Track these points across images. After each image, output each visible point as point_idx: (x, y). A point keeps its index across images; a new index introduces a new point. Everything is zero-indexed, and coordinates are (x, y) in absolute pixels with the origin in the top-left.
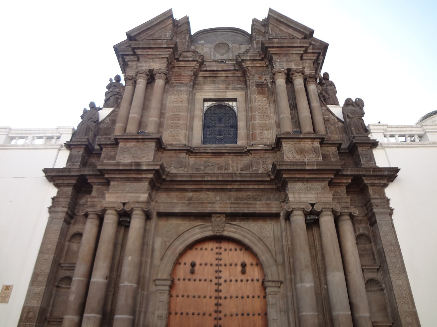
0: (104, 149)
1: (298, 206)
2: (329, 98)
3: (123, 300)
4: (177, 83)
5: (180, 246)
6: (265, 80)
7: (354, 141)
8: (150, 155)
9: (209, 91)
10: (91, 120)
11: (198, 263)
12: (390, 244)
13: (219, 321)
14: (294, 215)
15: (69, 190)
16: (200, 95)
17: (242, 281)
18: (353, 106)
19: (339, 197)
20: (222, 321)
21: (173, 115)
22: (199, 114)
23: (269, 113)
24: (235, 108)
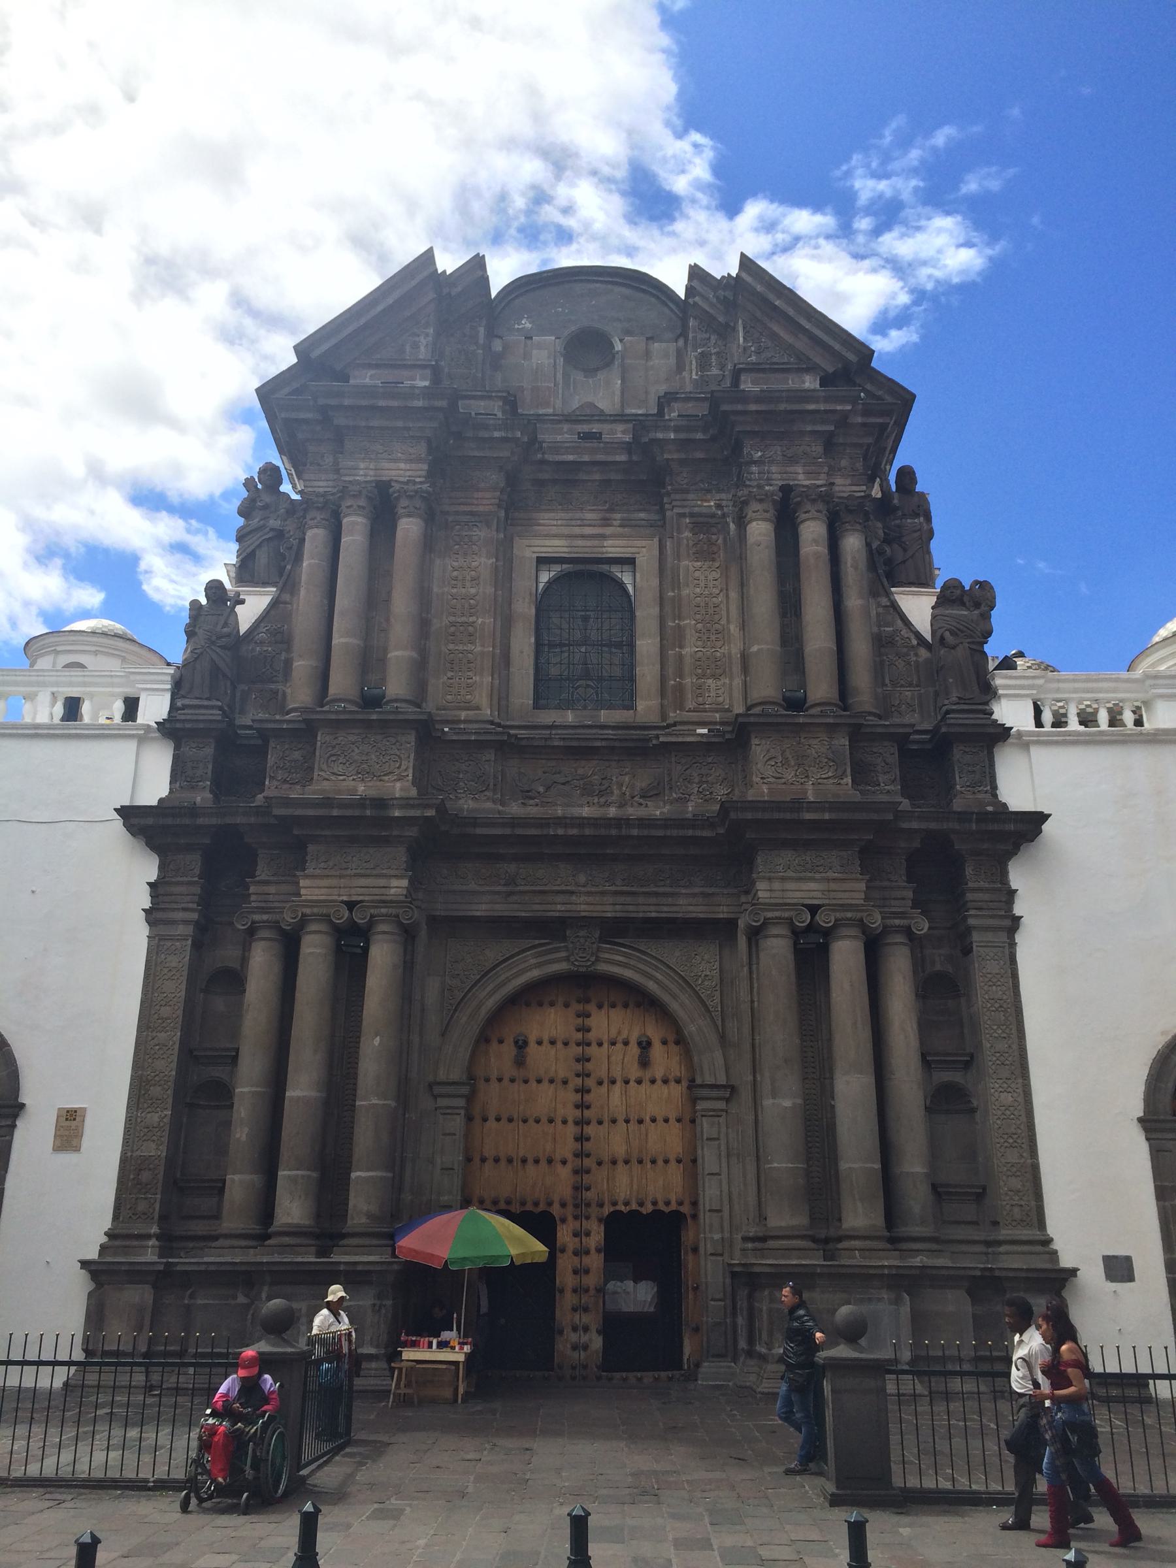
0: (272, 744)
1: (777, 914)
2: (904, 562)
3: (366, 1136)
4: (457, 513)
5: (489, 999)
6: (719, 506)
7: (944, 730)
8: (403, 767)
9: (555, 535)
10: (221, 642)
11: (532, 1039)
12: (997, 1005)
13: (585, 1111)
14: (766, 937)
15: (194, 863)
16: (528, 549)
17: (639, 1082)
18: (963, 604)
19: (886, 883)
20: (592, 1095)
21: (453, 624)
22: (525, 608)
23: (723, 622)
24: (630, 589)
